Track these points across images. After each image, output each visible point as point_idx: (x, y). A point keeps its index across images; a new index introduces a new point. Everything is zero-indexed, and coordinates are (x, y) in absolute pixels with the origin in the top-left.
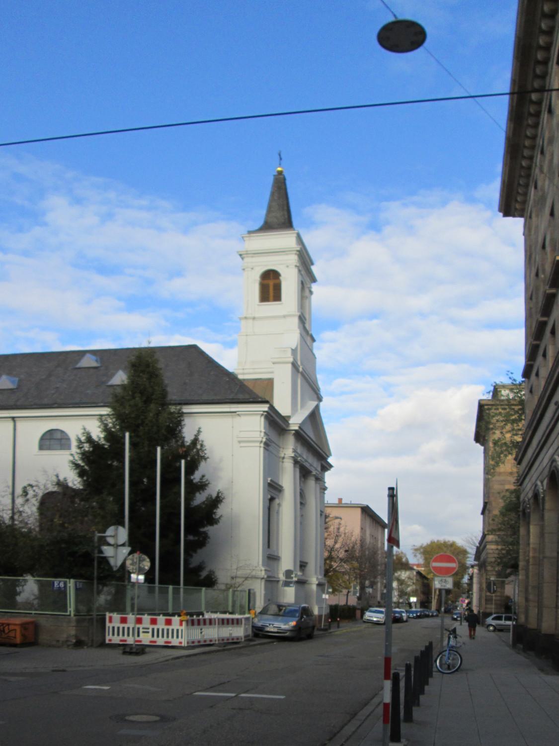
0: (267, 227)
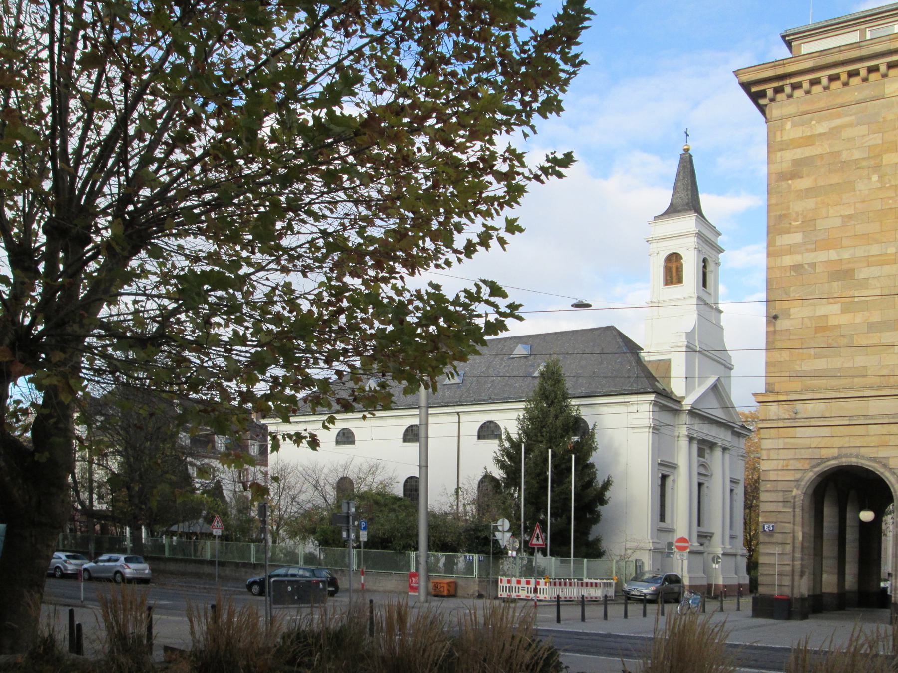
0: (673, 210)
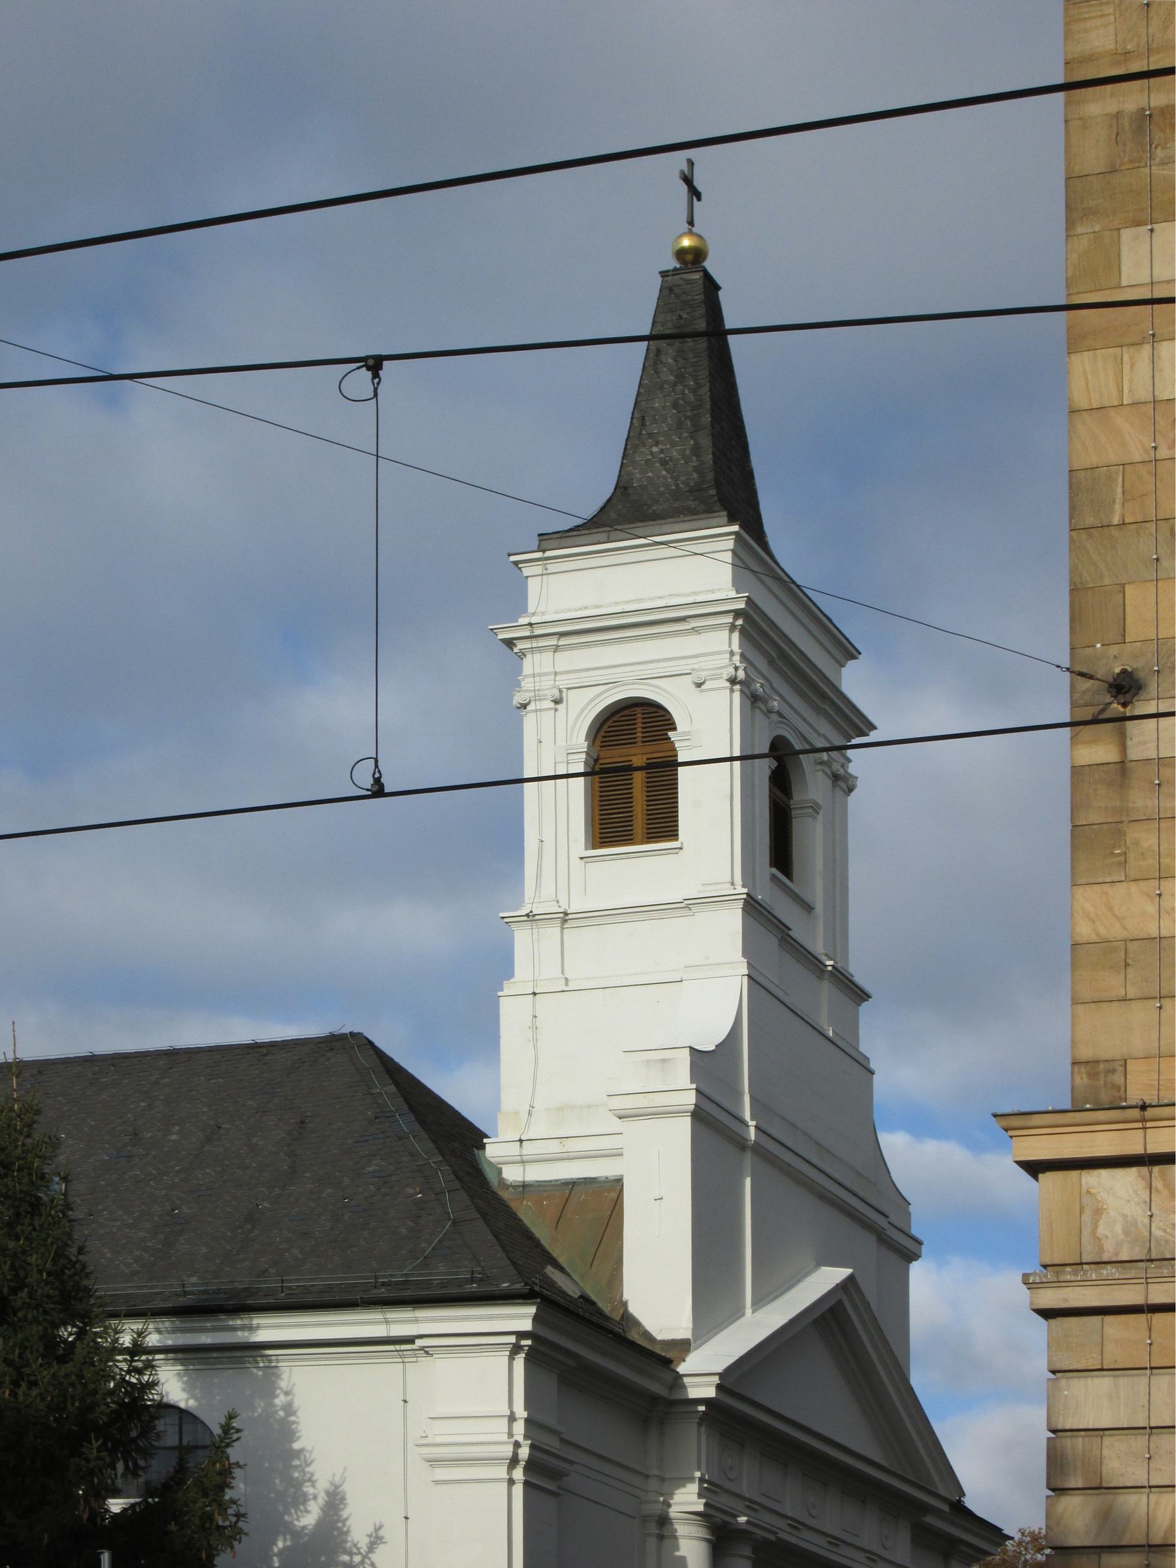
0: (628, 512)
